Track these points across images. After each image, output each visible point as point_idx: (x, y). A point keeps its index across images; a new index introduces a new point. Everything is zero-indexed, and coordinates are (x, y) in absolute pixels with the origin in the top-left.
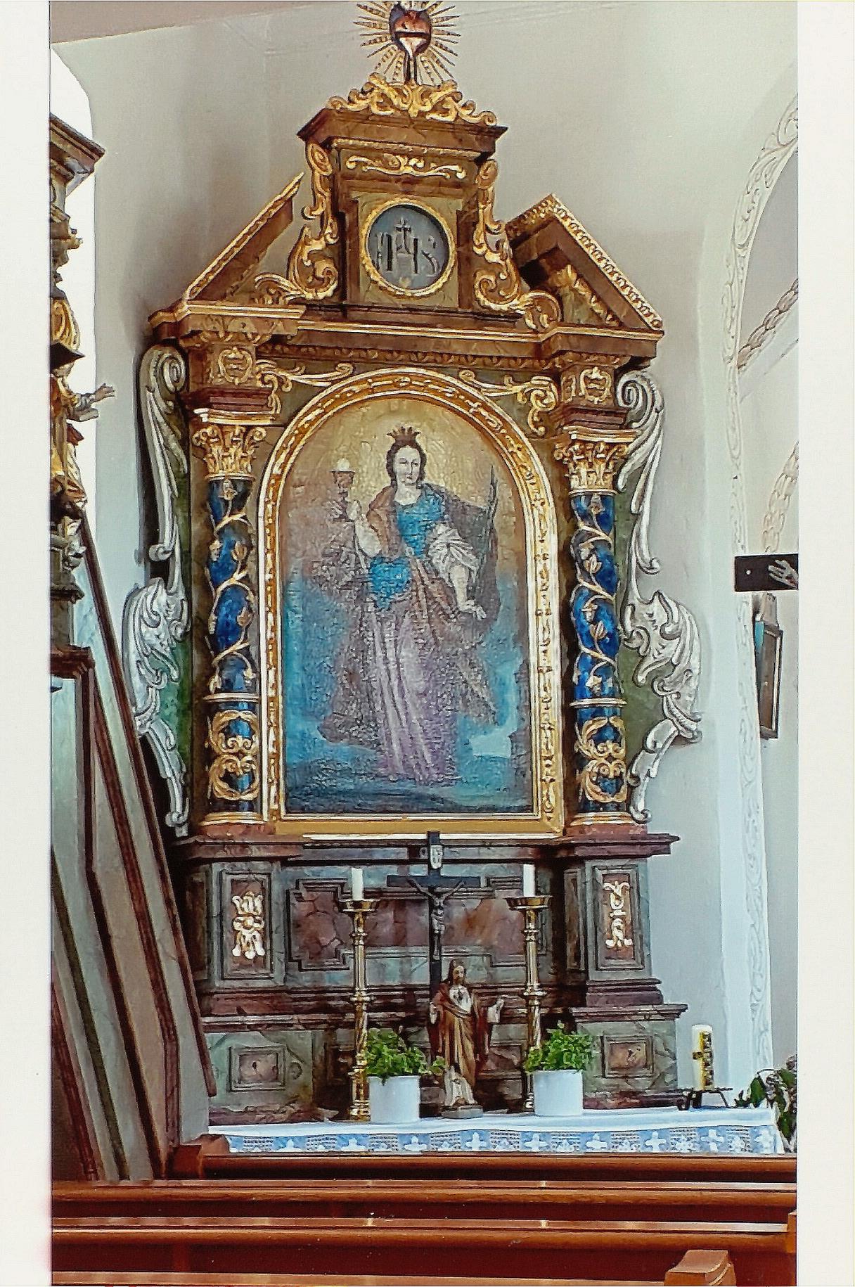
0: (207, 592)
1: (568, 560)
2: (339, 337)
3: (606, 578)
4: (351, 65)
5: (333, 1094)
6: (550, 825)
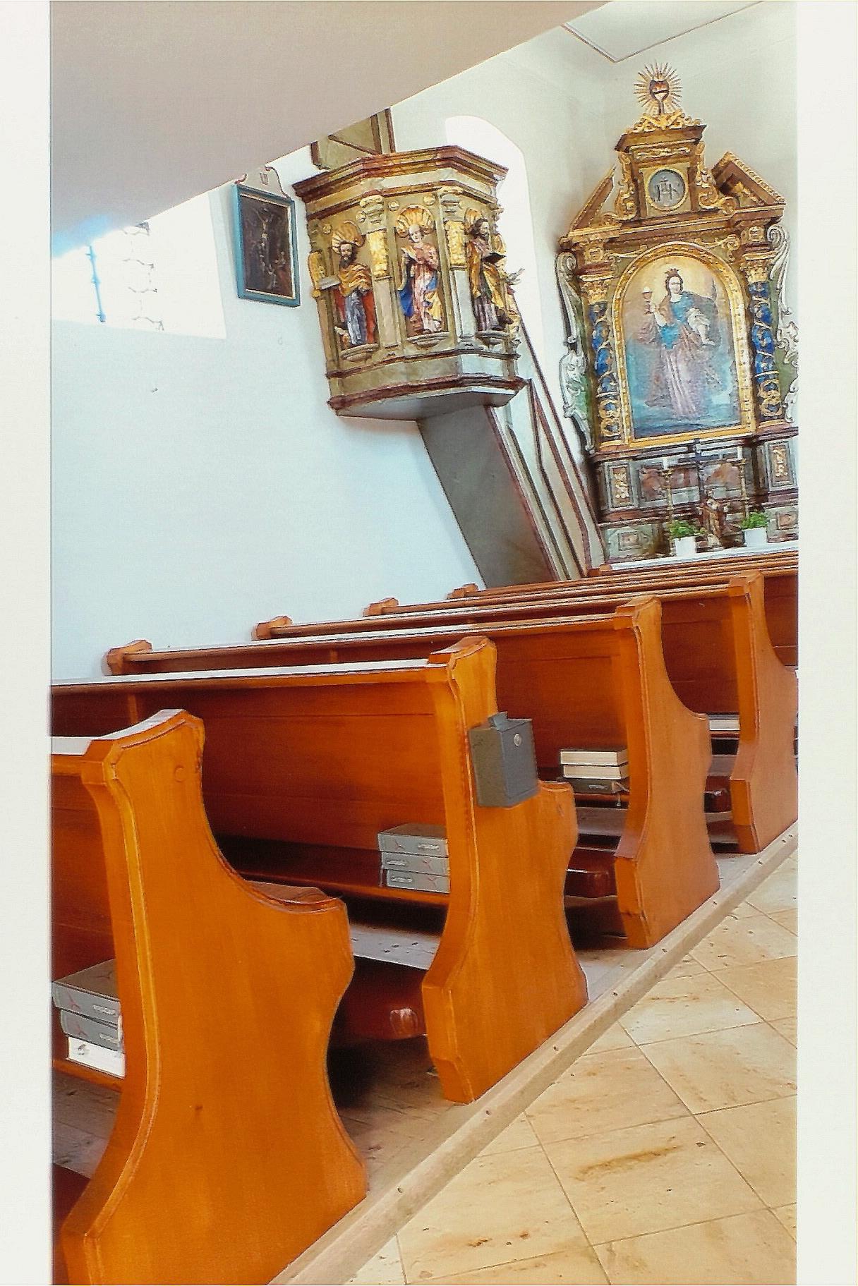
0: (593, 350)
1: (749, 315)
2: (639, 235)
3: (766, 319)
4: (636, 112)
5: (663, 547)
6: (750, 429)
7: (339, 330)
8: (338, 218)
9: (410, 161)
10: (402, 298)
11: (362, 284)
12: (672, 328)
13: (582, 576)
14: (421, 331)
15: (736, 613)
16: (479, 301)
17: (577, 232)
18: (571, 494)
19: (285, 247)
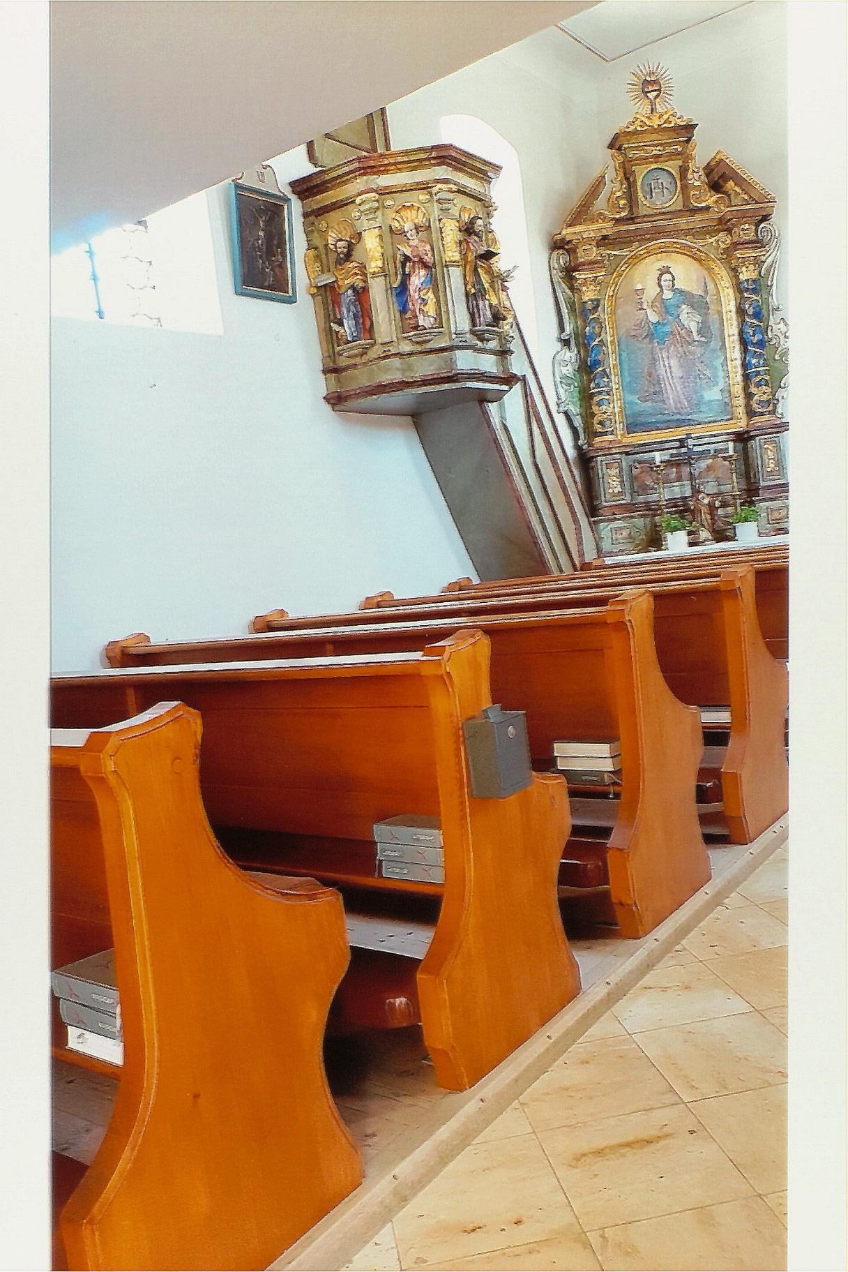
0: (586, 346)
1: (741, 312)
2: (632, 232)
3: (757, 315)
4: (628, 111)
5: (655, 541)
6: (741, 424)
7: (335, 327)
8: (334, 216)
9: (406, 159)
10: (397, 295)
11: (357, 281)
12: (664, 325)
13: (576, 570)
14: (416, 327)
15: (728, 606)
16: (473, 297)
17: (570, 230)
18: (564, 488)
19: (281, 244)
